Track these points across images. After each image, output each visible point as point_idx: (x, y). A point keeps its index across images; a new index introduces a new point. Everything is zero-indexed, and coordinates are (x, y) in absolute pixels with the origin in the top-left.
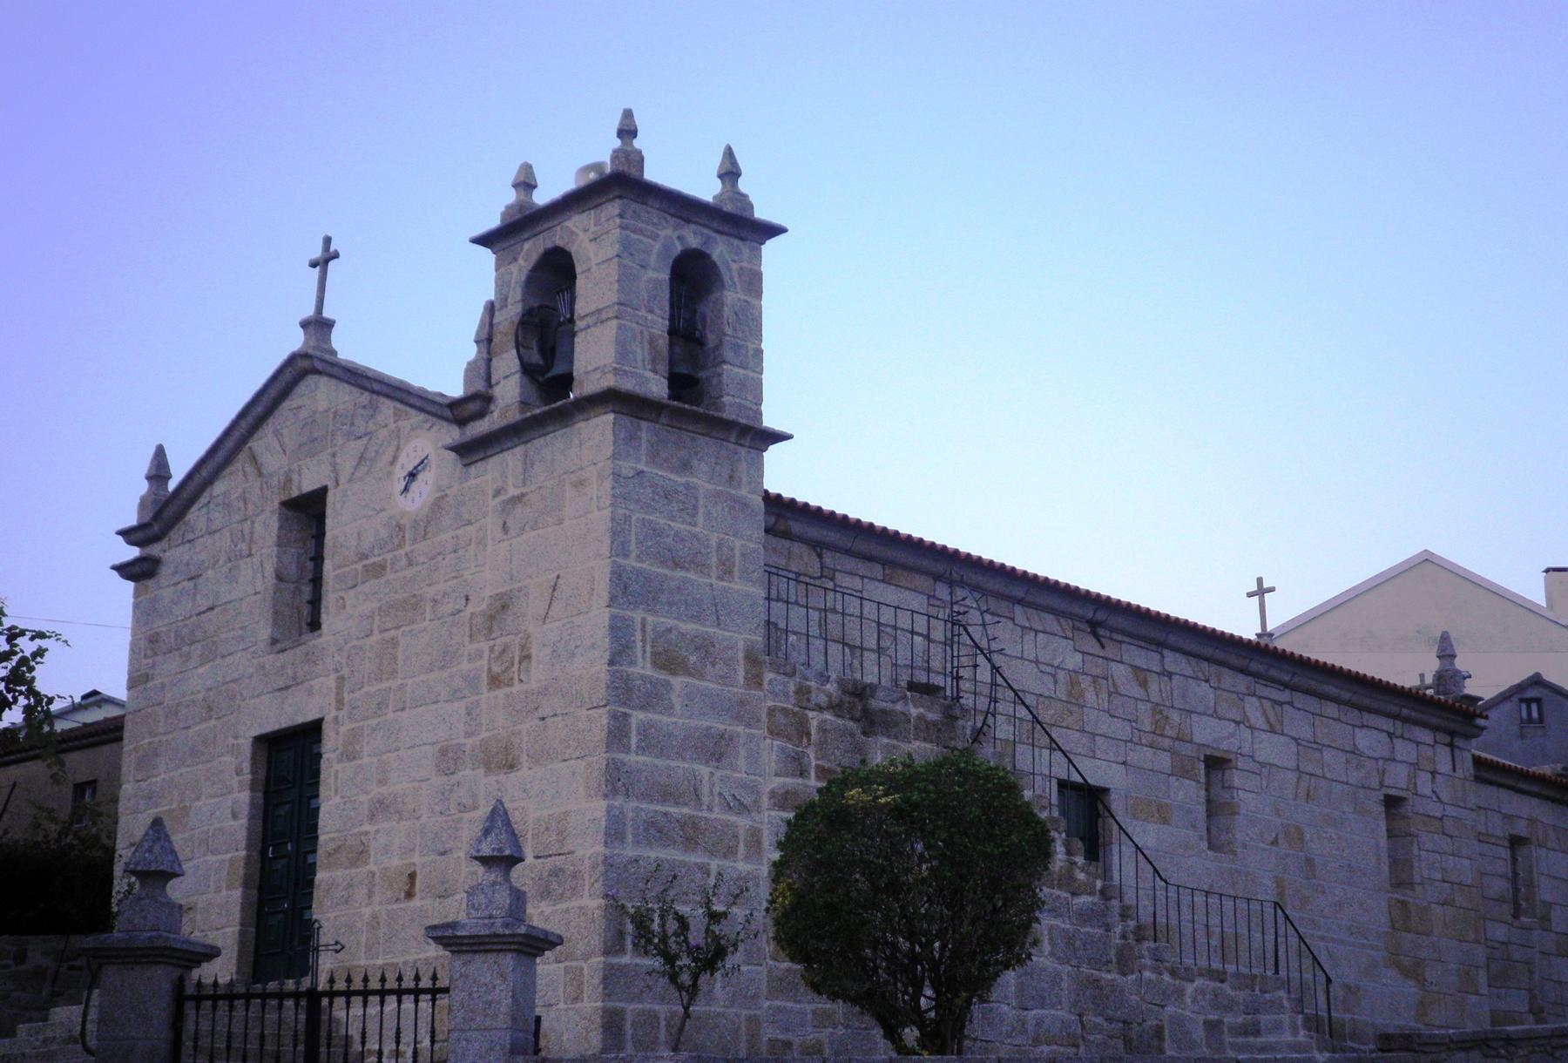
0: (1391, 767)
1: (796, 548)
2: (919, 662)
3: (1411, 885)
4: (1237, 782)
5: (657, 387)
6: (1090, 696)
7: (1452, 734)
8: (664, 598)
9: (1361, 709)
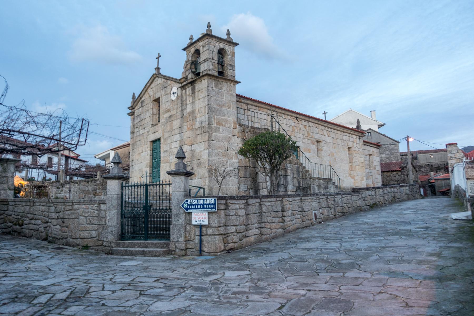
0: (349, 142)
1: (243, 104)
2: (265, 124)
3: (352, 163)
4: (322, 145)
5: (216, 74)
6: (296, 130)
7: (360, 136)
8: (218, 112)
9: (344, 132)
